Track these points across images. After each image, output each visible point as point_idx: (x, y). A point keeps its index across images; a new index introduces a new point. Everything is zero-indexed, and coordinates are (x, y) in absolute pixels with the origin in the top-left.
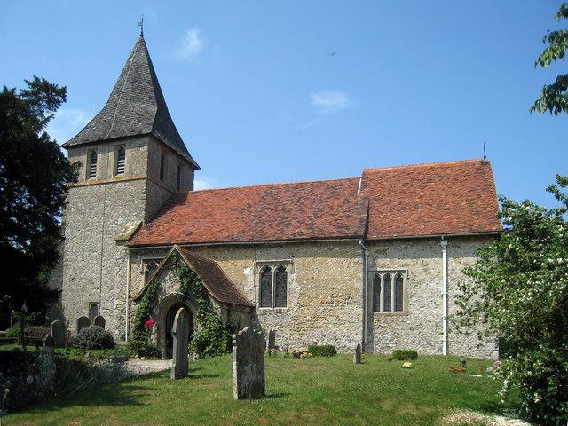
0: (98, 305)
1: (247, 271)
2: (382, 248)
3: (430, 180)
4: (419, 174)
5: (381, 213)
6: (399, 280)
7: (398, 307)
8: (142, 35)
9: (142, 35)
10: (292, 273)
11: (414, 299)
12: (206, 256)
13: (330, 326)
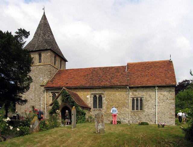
0: (35, 107)
2: (135, 90)
4: (147, 65)
5: (134, 78)
6: (141, 100)
7: (141, 109)
8: (44, 13)
9: (44, 13)
10: (104, 97)
12: (73, 91)
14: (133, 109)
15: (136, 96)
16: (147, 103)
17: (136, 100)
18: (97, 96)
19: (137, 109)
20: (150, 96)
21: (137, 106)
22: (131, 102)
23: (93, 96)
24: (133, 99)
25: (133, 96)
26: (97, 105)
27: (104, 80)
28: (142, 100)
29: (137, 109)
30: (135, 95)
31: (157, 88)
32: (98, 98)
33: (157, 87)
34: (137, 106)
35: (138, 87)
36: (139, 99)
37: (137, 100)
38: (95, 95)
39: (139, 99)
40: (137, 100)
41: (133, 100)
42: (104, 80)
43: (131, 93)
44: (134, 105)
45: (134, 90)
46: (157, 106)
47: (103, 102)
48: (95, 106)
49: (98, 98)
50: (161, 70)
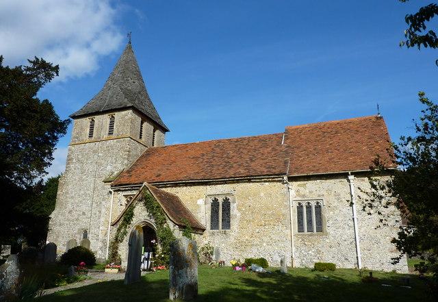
1: (201, 202)
2: (302, 183)
3: (337, 132)
4: (329, 128)
5: (301, 157)
6: (318, 207)
7: (320, 229)
8: (130, 43)
9: (130, 43)
10: (234, 202)
11: (331, 222)
12: (168, 190)
13: (265, 244)
14: (301, 229)
15: (305, 199)
16: (331, 212)
17: (307, 207)
18: (221, 200)
19: (310, 229)
20: (337, 196)
21: (310, 222)
22: (294, 211)
23: (210, 201)
24: (299, 204)
25: (300, 199)
26: (218, 218)
27: (234, 165)
28: (320, 206)
29: (310, 229)
30: (304, 196)
31: (351, 177)
32: (221, 204)
33: (352, 174)
34: (310, 222)
35: (308, 178)
36: (313, 204)
37: (309, 207)
38: (215, 199)
39: (313, 204)
40: (309, 207)
41: (300, 207)
42: (234, 165)
43: (292, 192)
44: (302, 219)
45: (299, 183)
46: (355, 220)
47: (231, 213)
48: (214, 225)
49: (221, 204)
50: (357, 137)
